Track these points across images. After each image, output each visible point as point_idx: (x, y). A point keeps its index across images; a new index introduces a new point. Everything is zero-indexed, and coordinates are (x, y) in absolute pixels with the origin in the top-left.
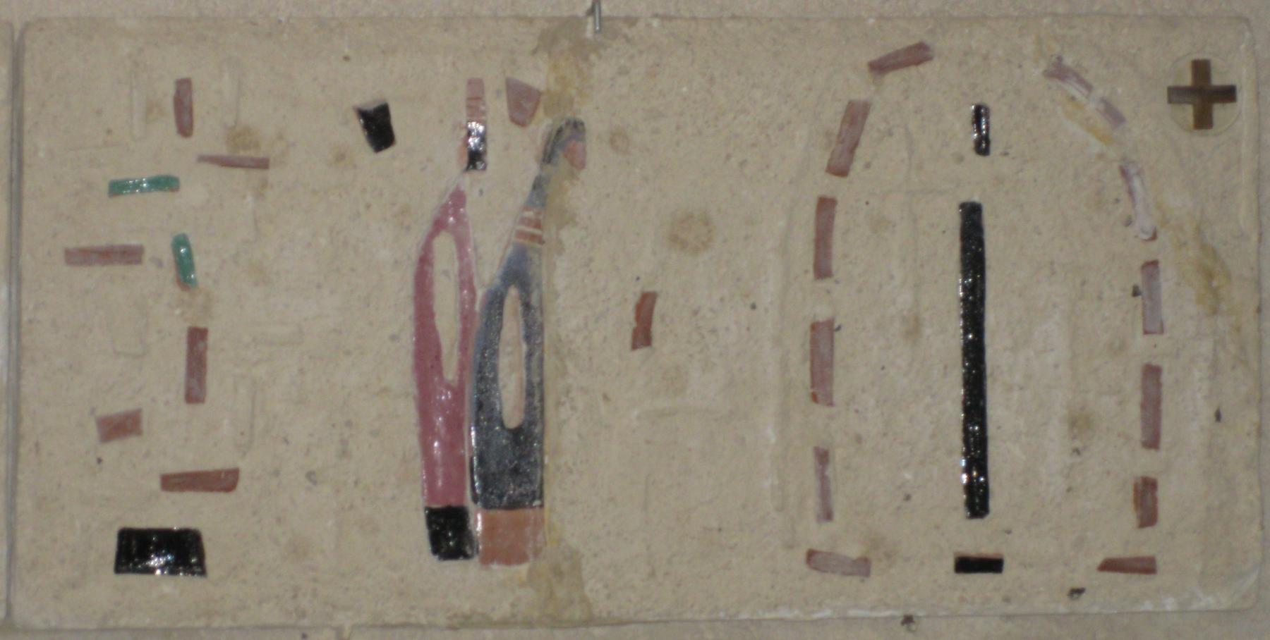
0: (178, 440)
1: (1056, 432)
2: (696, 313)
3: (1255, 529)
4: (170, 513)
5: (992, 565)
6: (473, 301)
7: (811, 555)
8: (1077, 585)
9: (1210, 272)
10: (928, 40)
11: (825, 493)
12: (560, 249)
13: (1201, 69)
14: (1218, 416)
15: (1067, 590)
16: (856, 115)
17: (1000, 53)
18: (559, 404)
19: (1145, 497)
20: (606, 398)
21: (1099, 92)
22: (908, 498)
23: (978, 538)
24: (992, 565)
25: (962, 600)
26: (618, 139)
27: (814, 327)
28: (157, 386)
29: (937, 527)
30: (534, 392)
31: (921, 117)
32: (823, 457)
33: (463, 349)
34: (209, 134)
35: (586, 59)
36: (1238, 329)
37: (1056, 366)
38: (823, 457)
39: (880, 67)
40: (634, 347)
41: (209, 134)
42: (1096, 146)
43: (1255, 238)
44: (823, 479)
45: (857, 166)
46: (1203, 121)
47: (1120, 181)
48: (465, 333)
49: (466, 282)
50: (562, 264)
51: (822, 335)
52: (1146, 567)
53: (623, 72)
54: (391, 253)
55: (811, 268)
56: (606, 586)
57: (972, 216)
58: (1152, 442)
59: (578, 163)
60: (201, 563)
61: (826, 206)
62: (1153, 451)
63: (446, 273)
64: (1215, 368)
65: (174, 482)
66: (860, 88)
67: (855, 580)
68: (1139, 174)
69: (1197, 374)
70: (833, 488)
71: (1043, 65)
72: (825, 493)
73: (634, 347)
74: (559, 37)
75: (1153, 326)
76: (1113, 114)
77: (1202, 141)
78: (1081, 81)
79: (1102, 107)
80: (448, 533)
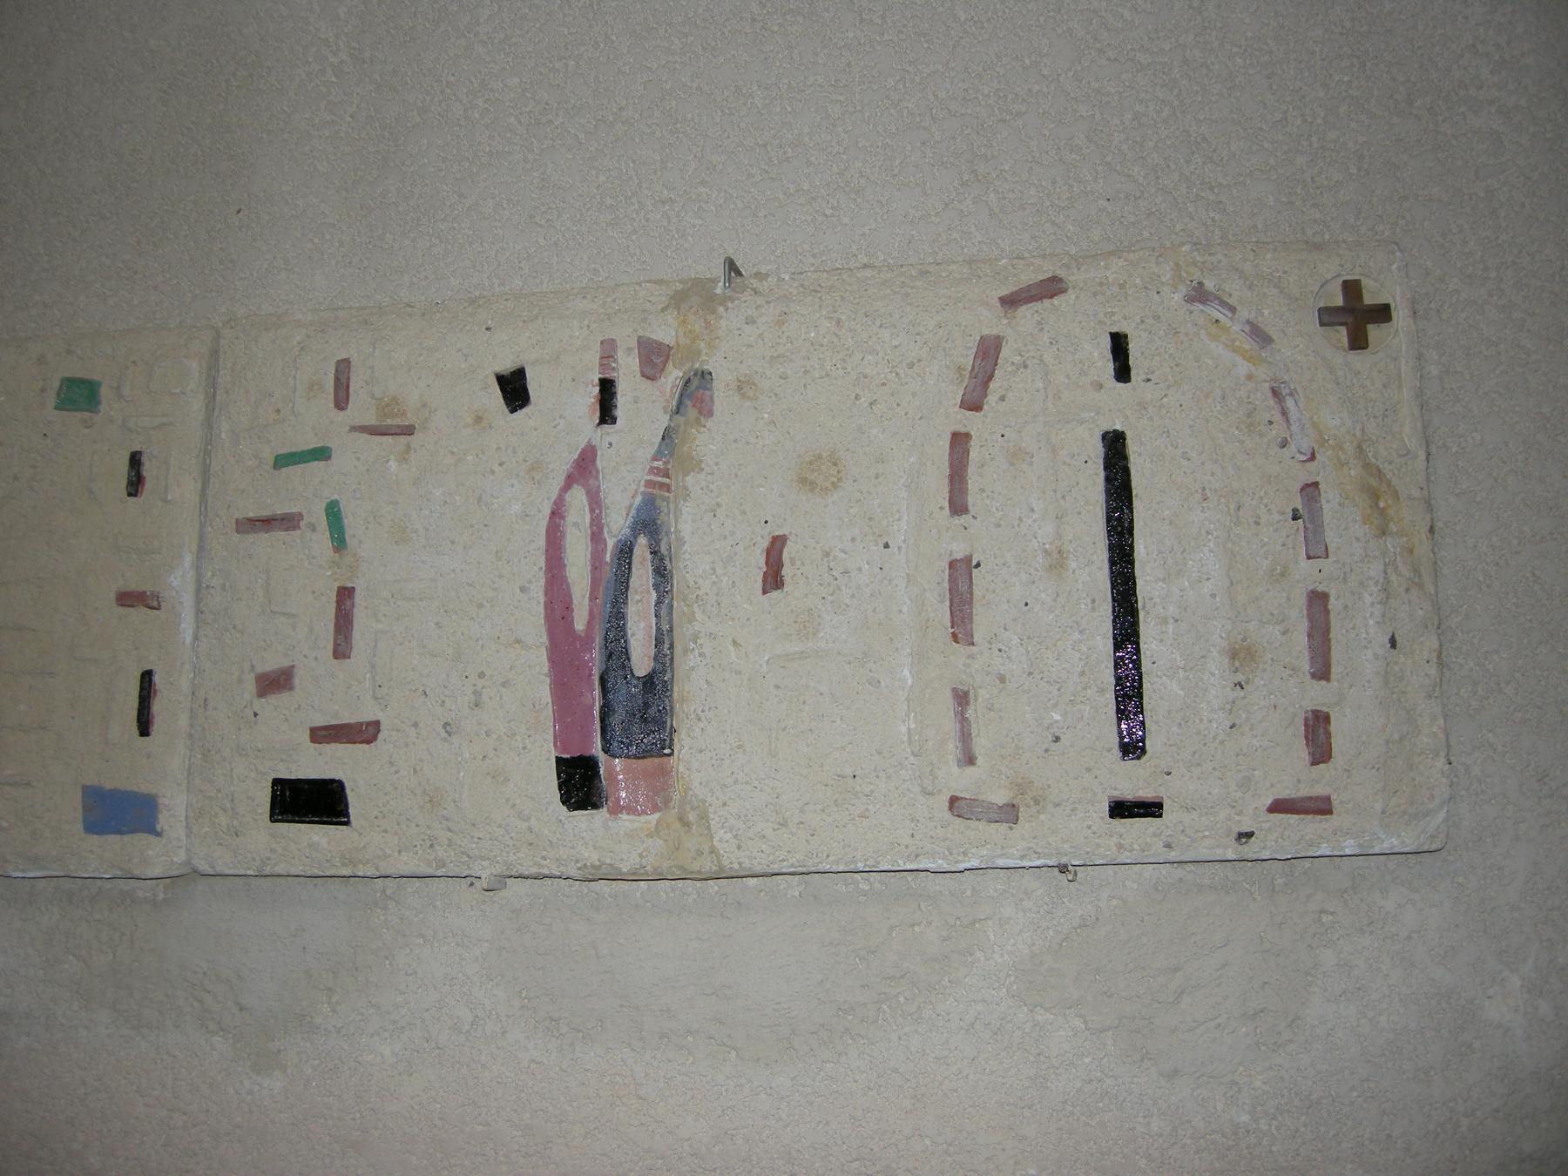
0: (329, 693)
1: (1216, 664)
2: (827, 554)
3: (1441, 763)
4: (313, 764)
5: (1152, 809)
6: (604, 550)
7: (953, 800)
8: (1245, 829)
9: (1376, 492)
10: (1061, 273)
11: (965, 737)
12: (686, 497)
13: (1352, 289)
14: (1393, 643)
15: (1235, 835)
16: (989, 351)
17: (1138, 281)
18: (685, 651)
19: (1317, 727)
20: (735, 643)
21: (1244, 313)
22: (1057, 739)
23: (1134, 781)
24: (1152, 809)
25: (1120, 847)
26: (744, 387)
27: (952, 565)
28: (304, 638)
29: (1089, 770)
30: (663, 640)
31: (1067, 340)
32: (962, 698)
33: (593, 598)
34: (362, 409)
35: (714, 312)
36: (1411, 551)
37: (1213, 596)
38: (962, 698)
39: (1010, 302)
40: (765, 592)
41: (362, 409)
42: (1243, 367)
43: (1423, 457)
44: (963, 721)
45: (992, 399)
46: (1358, 342)
47: (1272, 402)
48: (595, 583)
49: (597, 536)
50: (687, 509)
51: (961, 571)
52: (1321, 807)
53: (750, 321)
54: (521, 508)
55: (947, 505)
56: (735, 836)
57: (1115, 445)
58: (1322, 672)
59: (706, 411)
60: (347, 815)
61: (960, 441)
62: (1323, 683)
63: (576, 524)
64: (1386, 589)
65: (324, 734)
66: (990, 321)
67: (1003, 827)
68: (1291, 394)
69: (1368, 599)
70: (974, 732)
71: (1183, 290)
72: (965, 737)
73: (765, 592)
74: (695, 297)
75: (1316, 550)
76: (1260, 335)
77: (1358, 359)
78: (1223, 303)
79: (1247, 328)
80: (579, 783)
